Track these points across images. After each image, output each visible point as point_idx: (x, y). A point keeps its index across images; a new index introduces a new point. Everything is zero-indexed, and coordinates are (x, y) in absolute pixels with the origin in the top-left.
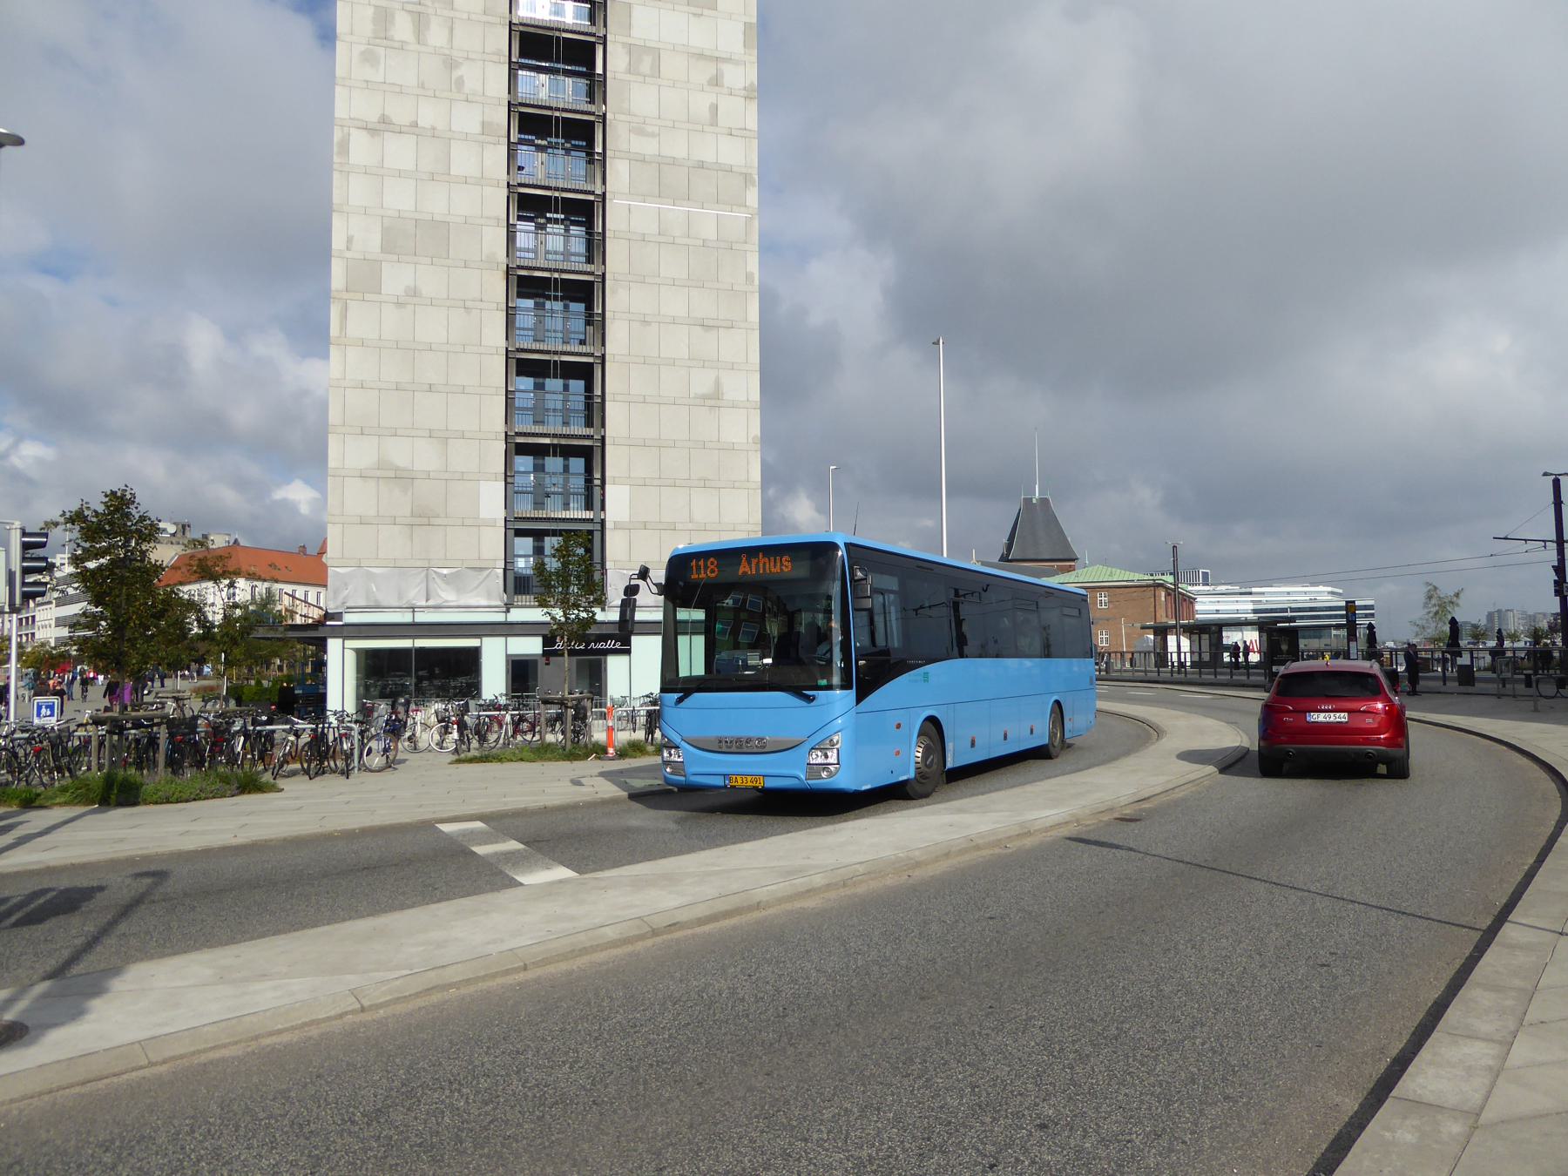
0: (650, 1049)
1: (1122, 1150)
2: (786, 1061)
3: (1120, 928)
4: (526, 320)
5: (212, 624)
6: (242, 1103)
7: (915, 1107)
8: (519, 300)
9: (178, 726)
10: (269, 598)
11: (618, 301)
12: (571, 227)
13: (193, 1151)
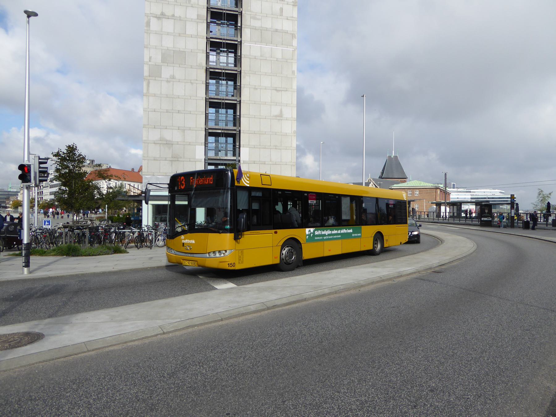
0: (273, 353)
1: (466, 402)
2: (325, 360)
3: (444, 313)
4: (212, 88)
5: (103, 194)
6: (122, 367)
7: (380, 380)
8: (210, 80)
9: (93, 229)
10: (121, 187)
11: (246, 81)
12: (229, 54)
13: (106, 385)
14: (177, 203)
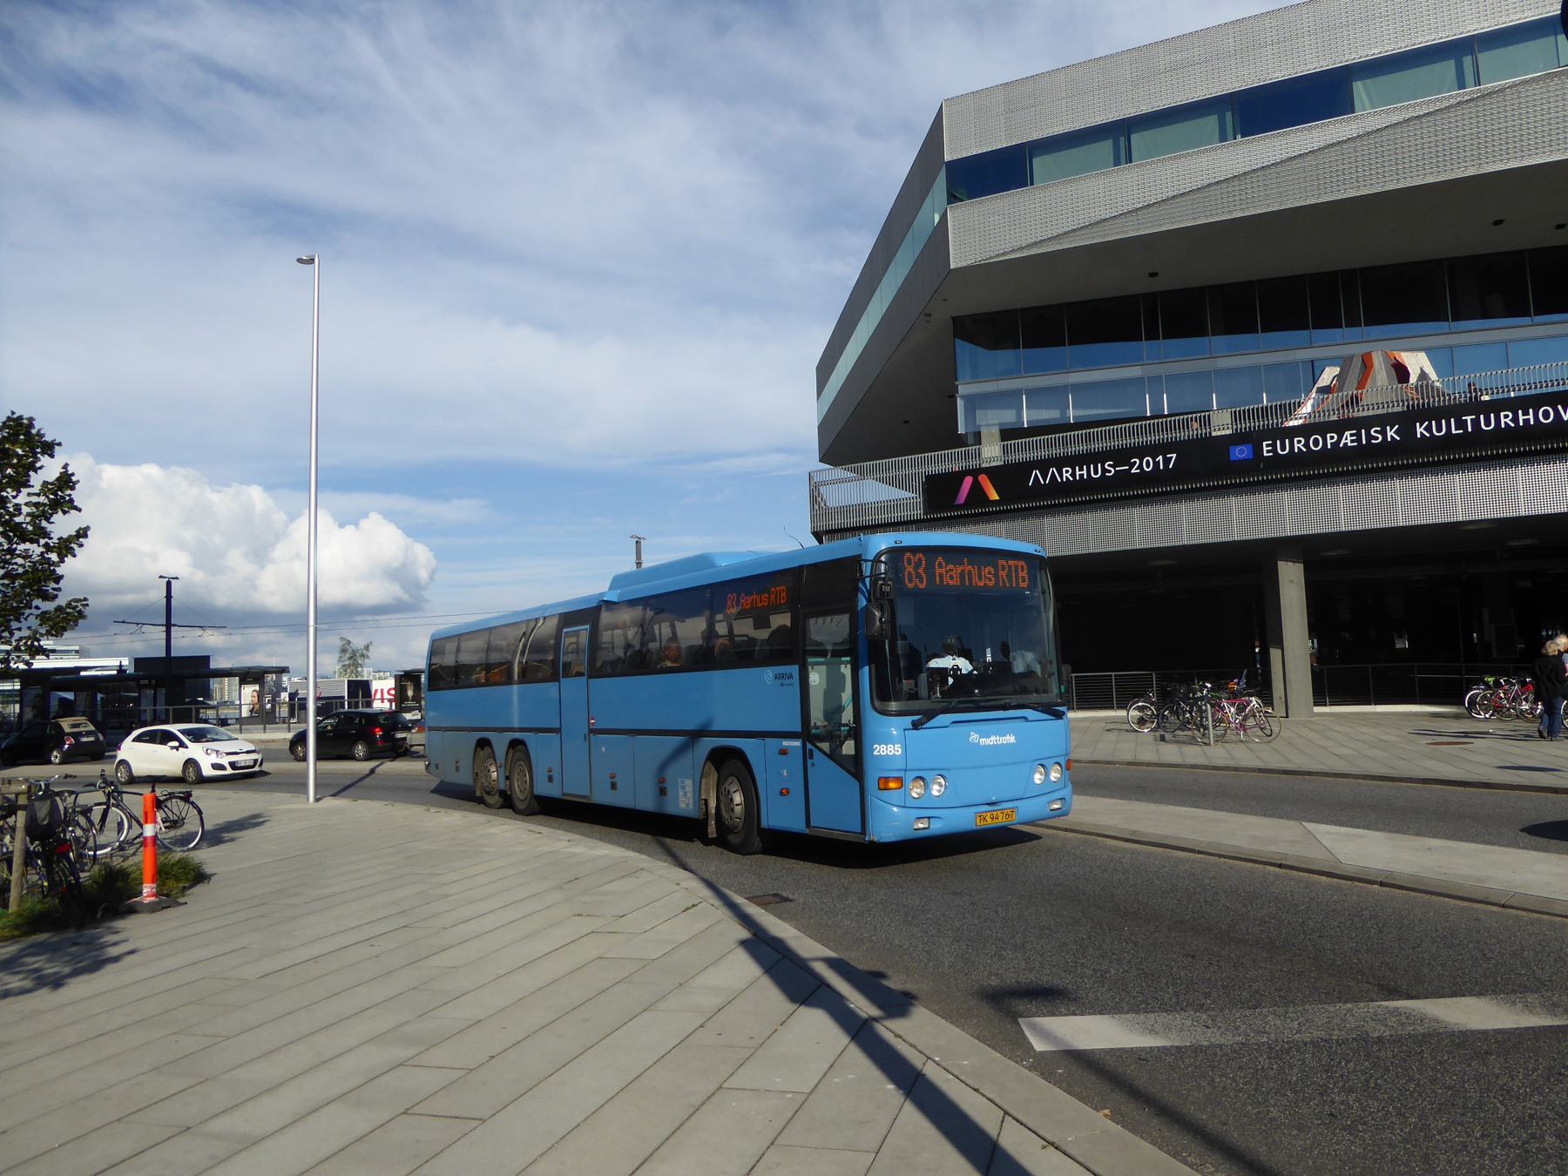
14: (137, 695)
